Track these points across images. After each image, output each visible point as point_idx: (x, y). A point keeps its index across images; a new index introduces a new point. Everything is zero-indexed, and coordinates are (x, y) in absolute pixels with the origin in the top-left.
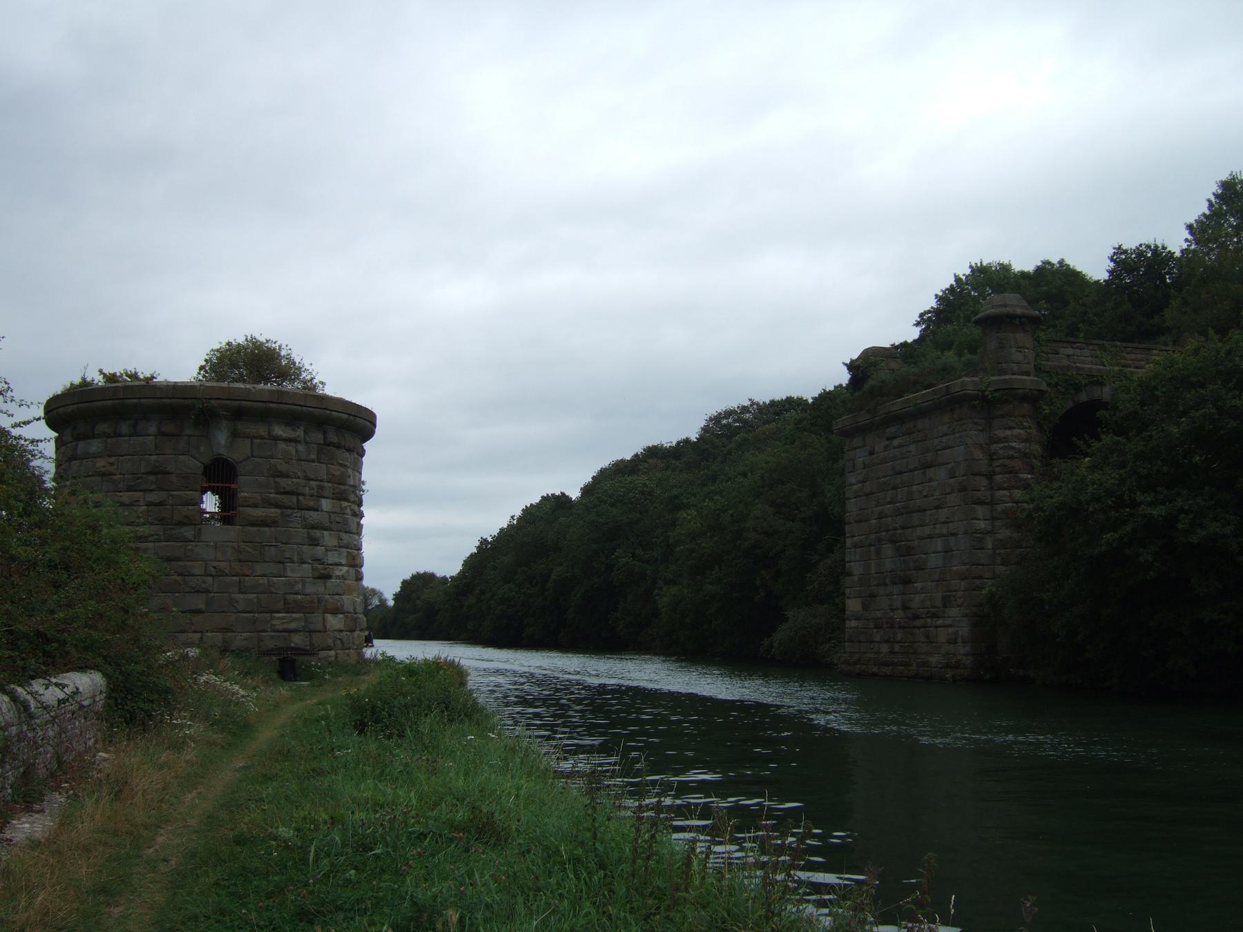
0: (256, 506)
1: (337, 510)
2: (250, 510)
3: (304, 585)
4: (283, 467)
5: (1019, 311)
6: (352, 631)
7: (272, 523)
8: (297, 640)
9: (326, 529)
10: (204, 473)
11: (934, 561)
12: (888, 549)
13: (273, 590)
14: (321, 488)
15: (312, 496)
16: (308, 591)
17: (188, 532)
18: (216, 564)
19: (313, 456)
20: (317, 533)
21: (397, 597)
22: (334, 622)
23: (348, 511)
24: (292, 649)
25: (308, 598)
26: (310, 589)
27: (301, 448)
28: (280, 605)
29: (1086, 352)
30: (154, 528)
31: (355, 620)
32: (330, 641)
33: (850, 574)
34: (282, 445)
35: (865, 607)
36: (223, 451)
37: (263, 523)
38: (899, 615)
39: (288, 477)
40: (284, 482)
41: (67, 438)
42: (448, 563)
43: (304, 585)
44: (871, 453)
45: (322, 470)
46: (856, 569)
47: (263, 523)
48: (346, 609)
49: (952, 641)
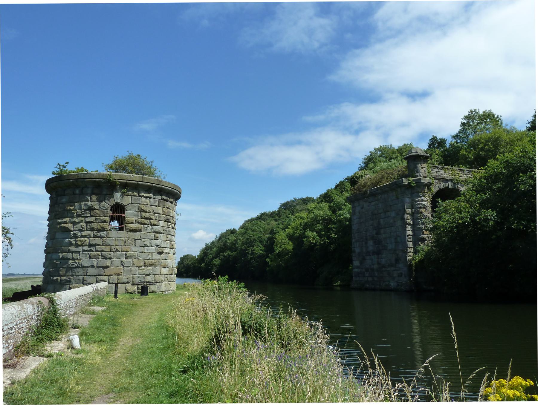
0: (132, 223)
1: (166, 226)
2: (130, 225)
3: (152, 256)
4: (144, 208)
5: (422, 154)
6: (171, 275)
7: (140, 231)
8: (149, 279)
9: (161, 233)
10: (111, 210)
11: (390, 246)
12: (371, 243)
13: (139, 258)
14: (159, 217)
15: (156, 220)
16: (153, 258)
17: (103, 234)
18: (115, 247)
19: (157, 204)
20: (158, 235)
21: (293, 249)
22: (164, 271)
23: (170, 226)
24: (147, 282)
25: (154, 261)
26: (154, 257)
27: (152, 200)
28: (142, 264)
29: (442, 171)
30: (89, 232)
31: (173, 270)
32: (163, 279)
33: (354, 252)
34: (143, 199)
35: (361, 263)
36: (119, 201)
37: (135, 231)
38: (376, 267)
39: (146, 212)
40: (144, 214)
41: (54, 196)
42: (196, 251)
43: (152, 256)
44: (362, 208)
45: (160, 210)
46: (357, 250)
47: (135, 231)
48: (169, 265)
49: (400, 275)
